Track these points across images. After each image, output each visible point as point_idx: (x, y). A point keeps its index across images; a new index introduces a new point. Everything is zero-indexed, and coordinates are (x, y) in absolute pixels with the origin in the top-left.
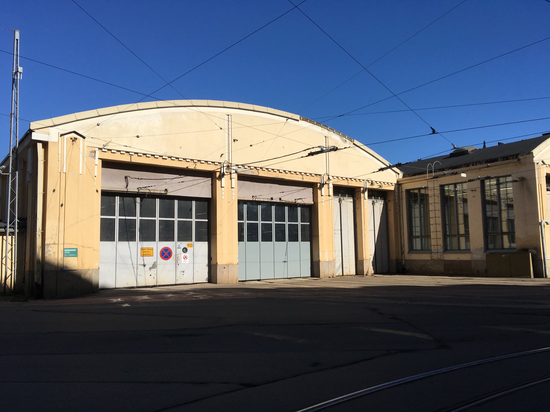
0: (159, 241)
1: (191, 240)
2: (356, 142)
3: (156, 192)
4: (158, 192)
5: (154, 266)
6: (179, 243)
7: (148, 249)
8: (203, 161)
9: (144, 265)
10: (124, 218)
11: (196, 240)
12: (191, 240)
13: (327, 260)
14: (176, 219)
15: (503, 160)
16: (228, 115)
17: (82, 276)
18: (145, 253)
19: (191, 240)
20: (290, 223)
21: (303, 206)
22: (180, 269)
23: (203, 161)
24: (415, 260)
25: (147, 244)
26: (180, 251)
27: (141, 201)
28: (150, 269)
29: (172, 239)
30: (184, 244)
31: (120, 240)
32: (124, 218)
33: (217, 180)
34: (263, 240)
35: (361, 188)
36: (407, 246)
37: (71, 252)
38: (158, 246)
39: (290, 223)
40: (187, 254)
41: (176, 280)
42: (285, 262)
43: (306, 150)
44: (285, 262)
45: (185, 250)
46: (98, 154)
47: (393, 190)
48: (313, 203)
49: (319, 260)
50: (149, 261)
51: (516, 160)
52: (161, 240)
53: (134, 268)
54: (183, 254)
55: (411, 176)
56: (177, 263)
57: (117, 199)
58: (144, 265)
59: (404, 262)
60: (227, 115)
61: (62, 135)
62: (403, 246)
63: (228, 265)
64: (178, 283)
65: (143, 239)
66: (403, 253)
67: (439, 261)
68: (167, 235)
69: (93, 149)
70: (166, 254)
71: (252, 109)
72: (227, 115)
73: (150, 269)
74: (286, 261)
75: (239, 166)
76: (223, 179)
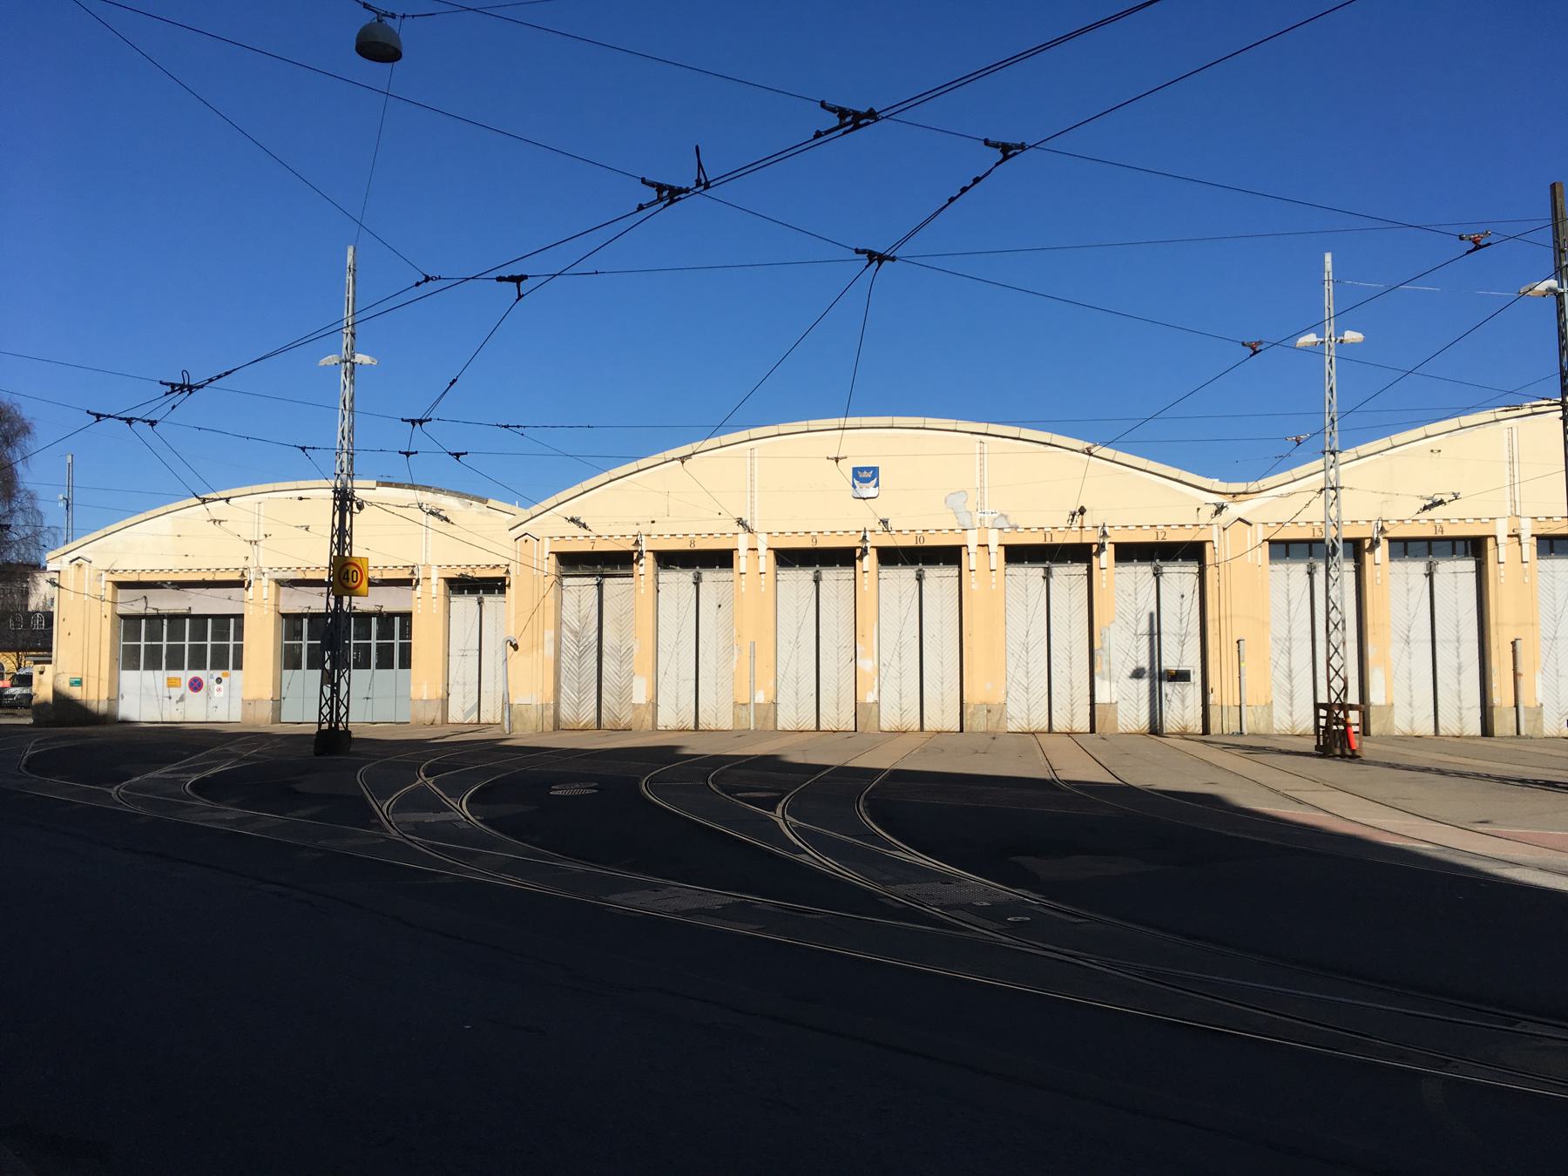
0: (308, 669)
1: (227, 668)
2: (492, 503)
3: (176, 612)
4: (179, 611)
5: (182, 699)
6: (212, 672)
7: (176, 679)
9: (170, 698)
10: (149, 643)
11: (234, 669)
12: (227, 668)
13: (425, 698)
14: (143, 643)
17: (88, 707)
18: (172, 683)
19: (227, 668)
20: (380, 641)
21: (313, 617)
22: (212, 704)
25: (174, 673)
26: (214, 681)
27: (169, 623)
28: (177, 702)
29: (204, 668)
30: (218, 673)
31: (145, 668)
32: (149, 643)
33: (1367, 553)
34: (379, 666)
36: (1494, 678)
37: (76, 682)
38: (186, 675)
39: (380, 641)
40: (221, 686)
41: (207, 717)
42: (367, 698)
44: (367, 698)
45: (219, 681)
46: (105, 576)
47: (1354, 547)
50: (176, 693)
52: (190, 668)
53: (158, 700)
54: (217, 686)
56: (209, 696)
57: (143, 621)
58: (170, 698)
61: (516, 540)
63: (255, 701)
64: (209, 720)
65: (169, 668)
68: (198, 663)
69: (100, 572)
70: (196, 685)
71: (295, 488)
73: (177, 702)
75: (1173, 527)
76: (1378, 551)
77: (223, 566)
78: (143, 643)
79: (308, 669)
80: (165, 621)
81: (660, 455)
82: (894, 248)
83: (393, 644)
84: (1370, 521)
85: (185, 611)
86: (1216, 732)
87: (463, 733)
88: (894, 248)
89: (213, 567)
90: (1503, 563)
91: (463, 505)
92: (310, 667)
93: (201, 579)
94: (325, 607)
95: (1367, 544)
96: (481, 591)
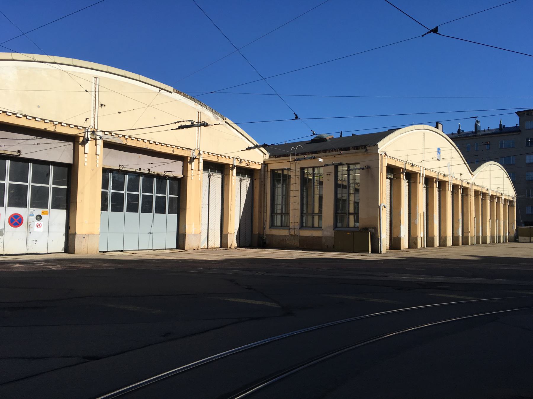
0: (31, 207)
3: (6, 152)
8: (65, 123)
15: (354, 149)
16: (96, 78)
22: (31, 237)
23: (65, 123)
24: (275, 235)
29: (24, 205)
30: (38, 211)
33: (80, 146)
34: (143, 211)
35: (230, 165)
39: (158, 195)
41: (27, 249)
42: (150, 233)
43: (177, 122)
44: (150, 233)
45: (39, 217)
48: (182, 176)
49: (185, 233)
51: (364, 150)
52: (10, 205)
54: (37, 222)
55: (277, 157)
56: (28, 231)
59: (266, 236)
60: (95, 78)
62: (265, 222)
64: (28, 252)
66: (264, 229)
67: (295, 236)
72: (95, 78)
74: (152, 232)
77: (65, 121)
78: (51, 186)
79: (31, 207)
80: (155, 180)
81: (31, 55)
82: (506, 112)
83: (10, 180)
84: (233, 158)
85: (15, 154)
86: (449, 245)
87: (362, 256)
88: (506, 112)
89: (56, 119)
90: (87, 153)
91: (215, 117)
92: (55, 206)
93: (43, 128)
94: (13, 154)
95: (81, 139)
96: (216, 171)
